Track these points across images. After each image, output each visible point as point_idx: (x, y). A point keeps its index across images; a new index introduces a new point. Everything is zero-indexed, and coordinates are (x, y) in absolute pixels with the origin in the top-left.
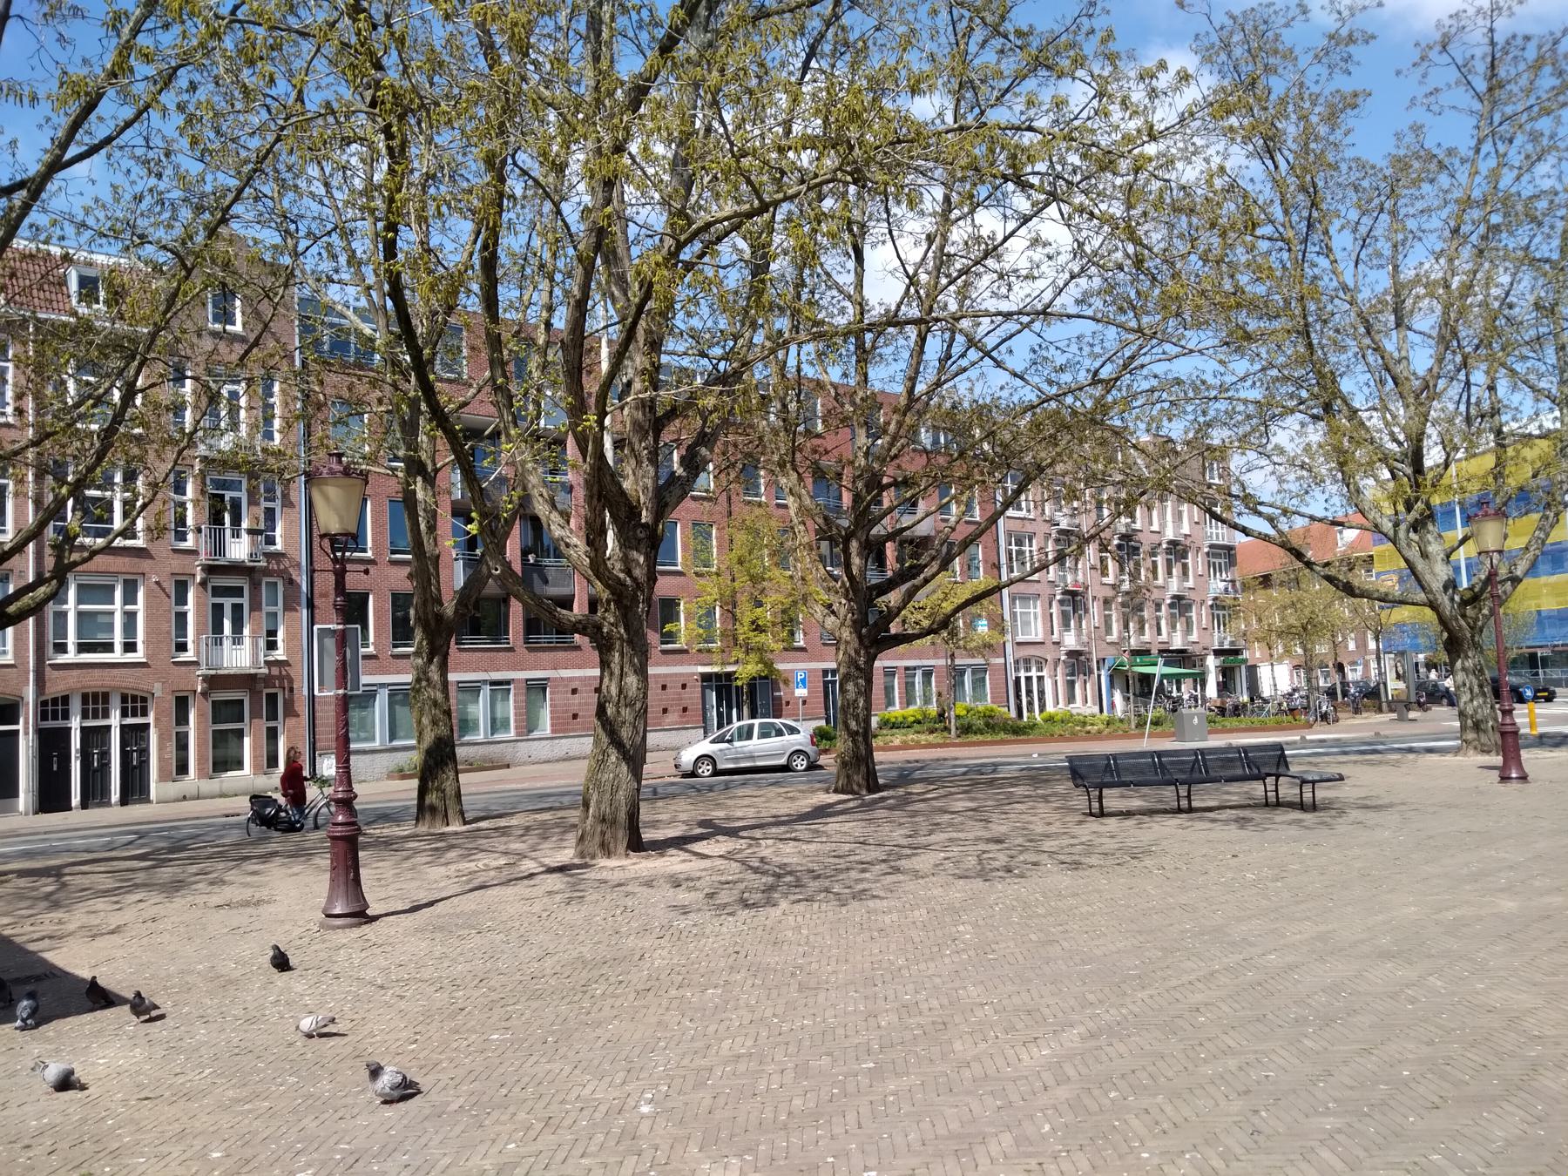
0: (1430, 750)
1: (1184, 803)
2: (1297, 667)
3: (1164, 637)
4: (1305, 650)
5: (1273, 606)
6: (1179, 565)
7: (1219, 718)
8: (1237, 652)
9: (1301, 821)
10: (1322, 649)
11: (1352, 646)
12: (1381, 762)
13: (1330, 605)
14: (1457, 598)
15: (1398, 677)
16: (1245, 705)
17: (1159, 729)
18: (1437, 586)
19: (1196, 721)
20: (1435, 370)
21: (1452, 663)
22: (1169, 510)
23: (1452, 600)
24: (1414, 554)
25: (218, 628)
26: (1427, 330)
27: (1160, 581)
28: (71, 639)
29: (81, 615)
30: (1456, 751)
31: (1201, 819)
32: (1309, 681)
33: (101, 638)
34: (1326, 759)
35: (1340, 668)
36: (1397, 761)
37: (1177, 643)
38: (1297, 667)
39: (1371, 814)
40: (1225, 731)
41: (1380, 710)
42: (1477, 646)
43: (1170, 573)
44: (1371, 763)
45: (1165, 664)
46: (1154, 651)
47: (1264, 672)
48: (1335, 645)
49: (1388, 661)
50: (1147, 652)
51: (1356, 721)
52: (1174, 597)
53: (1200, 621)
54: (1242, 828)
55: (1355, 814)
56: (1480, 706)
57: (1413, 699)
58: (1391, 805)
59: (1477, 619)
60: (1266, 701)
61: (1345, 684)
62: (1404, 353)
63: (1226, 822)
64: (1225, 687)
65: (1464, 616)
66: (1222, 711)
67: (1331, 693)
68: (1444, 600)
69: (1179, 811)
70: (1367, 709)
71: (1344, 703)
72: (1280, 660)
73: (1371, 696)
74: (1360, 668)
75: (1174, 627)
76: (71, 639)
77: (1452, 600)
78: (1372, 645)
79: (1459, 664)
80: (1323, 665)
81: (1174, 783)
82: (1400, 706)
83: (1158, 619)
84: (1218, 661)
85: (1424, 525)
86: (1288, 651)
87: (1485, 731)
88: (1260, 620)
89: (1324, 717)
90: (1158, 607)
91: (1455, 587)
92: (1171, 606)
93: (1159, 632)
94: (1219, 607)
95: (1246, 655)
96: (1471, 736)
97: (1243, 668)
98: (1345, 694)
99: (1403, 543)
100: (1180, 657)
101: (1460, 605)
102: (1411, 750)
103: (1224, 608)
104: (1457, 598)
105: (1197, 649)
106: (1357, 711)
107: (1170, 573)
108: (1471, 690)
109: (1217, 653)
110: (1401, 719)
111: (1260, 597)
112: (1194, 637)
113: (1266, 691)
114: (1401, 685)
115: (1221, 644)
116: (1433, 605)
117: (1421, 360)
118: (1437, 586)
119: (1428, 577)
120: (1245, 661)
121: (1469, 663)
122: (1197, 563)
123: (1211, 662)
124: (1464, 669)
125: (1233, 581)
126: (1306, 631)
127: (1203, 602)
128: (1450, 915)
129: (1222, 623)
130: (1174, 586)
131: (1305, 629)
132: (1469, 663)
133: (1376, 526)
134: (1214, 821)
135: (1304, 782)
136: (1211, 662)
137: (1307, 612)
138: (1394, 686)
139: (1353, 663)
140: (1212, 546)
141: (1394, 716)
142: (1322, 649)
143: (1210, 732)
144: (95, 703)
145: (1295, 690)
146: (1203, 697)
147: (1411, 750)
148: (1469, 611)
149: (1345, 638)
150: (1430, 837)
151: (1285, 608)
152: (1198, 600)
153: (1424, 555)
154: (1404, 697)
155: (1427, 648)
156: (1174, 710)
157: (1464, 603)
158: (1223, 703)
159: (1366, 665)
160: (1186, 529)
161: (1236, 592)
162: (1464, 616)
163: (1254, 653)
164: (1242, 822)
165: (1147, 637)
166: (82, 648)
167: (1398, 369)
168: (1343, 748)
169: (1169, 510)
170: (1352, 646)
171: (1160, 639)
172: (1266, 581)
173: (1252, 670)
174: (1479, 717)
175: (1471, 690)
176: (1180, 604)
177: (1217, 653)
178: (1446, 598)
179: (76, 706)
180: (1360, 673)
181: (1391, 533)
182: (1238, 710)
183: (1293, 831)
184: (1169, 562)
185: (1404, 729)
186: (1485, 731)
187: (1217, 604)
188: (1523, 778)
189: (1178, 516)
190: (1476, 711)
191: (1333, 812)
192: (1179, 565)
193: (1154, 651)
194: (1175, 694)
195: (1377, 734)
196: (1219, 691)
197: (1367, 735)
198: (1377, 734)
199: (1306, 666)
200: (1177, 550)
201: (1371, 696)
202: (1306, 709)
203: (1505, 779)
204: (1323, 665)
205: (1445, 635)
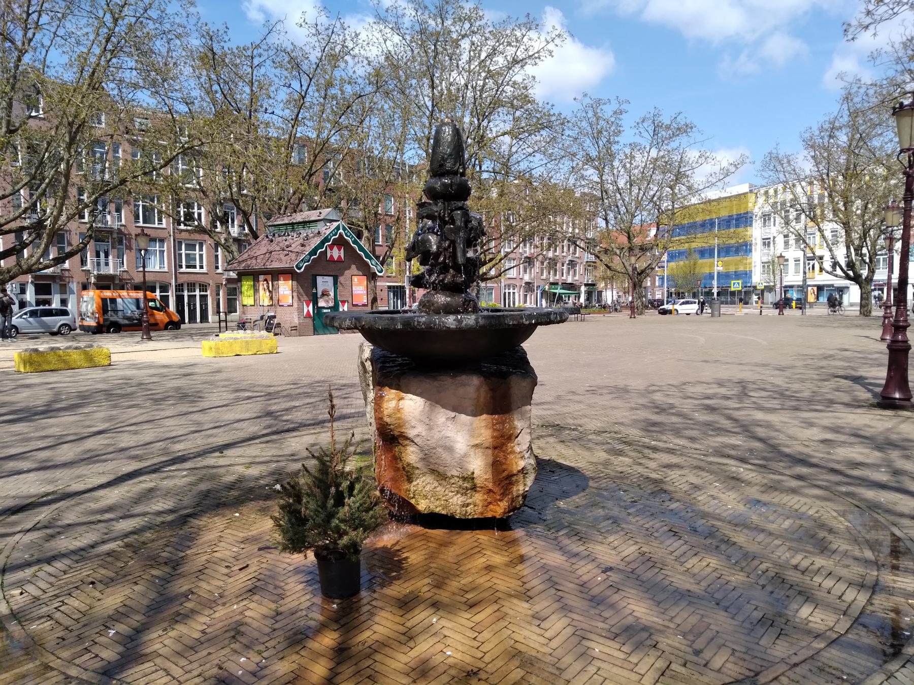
3: (564, 278)
28: (184, 264)
29: (186, 255)
33: (192, 263)
37: (570, 280)
50: (557, 284)
76: (184, 264)
100: (571, 287)
105: (577, 283)
109: (586, 285)
112: (576, 278)
123: (583, 289)
136: (583, 289)
144: (191, 286)
165: (557, 277)
166: (188, 267)
173: (600, 293)
177: (586, 285)
179: (185, 287)
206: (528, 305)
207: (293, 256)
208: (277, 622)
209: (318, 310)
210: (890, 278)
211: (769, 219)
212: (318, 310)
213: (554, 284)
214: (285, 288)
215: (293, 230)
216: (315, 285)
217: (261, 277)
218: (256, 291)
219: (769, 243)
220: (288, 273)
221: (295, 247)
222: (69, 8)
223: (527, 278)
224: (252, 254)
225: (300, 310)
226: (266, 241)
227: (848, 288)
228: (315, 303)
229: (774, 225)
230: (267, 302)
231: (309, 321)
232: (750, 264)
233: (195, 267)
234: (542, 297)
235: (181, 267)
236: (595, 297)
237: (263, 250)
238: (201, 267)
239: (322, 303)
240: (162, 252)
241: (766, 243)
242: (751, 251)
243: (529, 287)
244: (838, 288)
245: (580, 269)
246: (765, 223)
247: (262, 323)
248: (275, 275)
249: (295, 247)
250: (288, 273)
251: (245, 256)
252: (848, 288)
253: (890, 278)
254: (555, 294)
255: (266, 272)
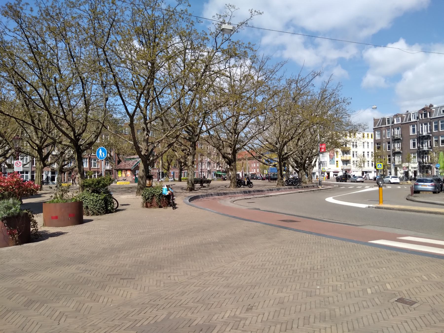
25: (106, 165)
28: (93, 165)
29: (94, 163)
33: (95, 165)
50: (220, 171)
76: (93, 165)
166: (94, 166)
206: (209, 178)
207: (131, 166)
209: (136, 178)
212: (136, 178)
214: (129, 173)
215: (130, 160)
216: (135, 172)
217: (123, 171)
218: (122, 173)
220: (130, 170)
221: (131, 164)
223: (208, 169)
224: (121, 165)
225: (132, 178)
226: (124, 162)
228: (135, 176)
230: (124, 176)
231: (134, 180)
233: (96, 166)
234: (214, 176)
235: (92, 166)
237: (123, 164)
238: (98, 166)
239: (137, 176)
240: (86, 162)
243: (209, 172)
247: (247, 25)
248: (127, 170)
249: (131, 164)
250: (130, 170)
251: (119, 166)
255: (124, 169)
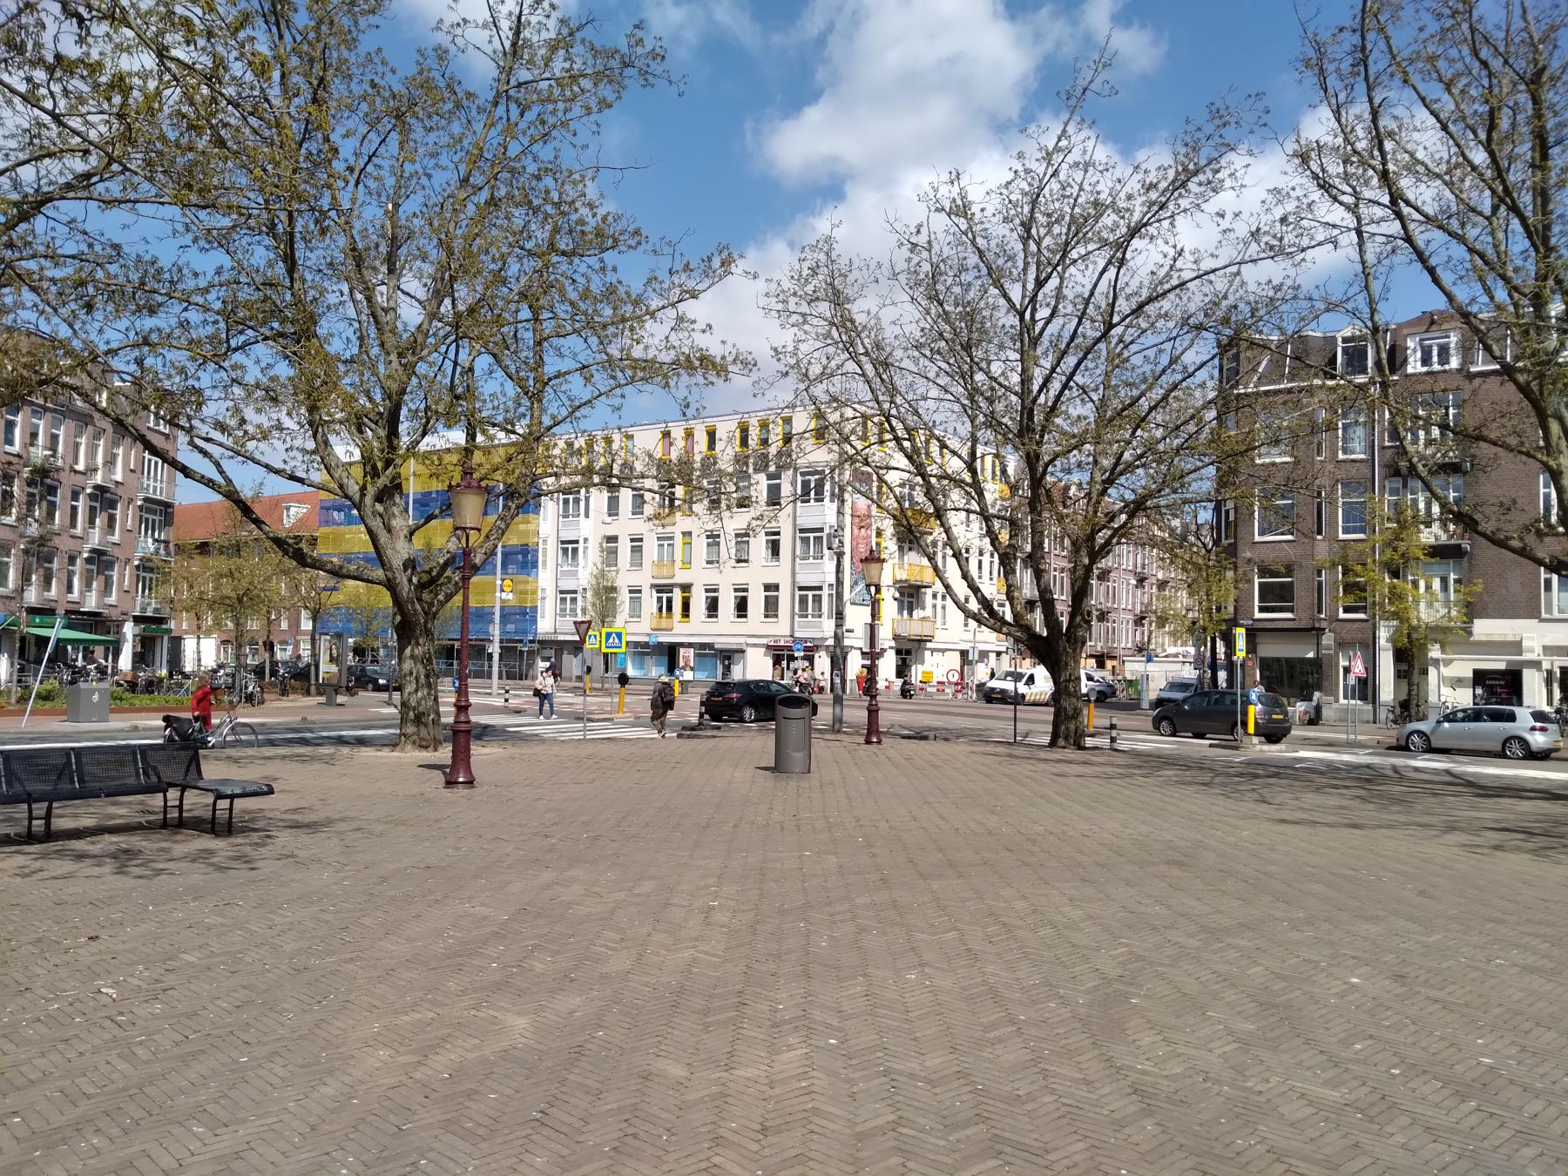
0: (361, 742)
1: (38, 825)
2: (225, 642)
3: (75, 595)
4: (237, 625)
5: (206, 574)
6: (105, 515)
7: (128, 695)
8: (161, 621)
9: (210, 852)
10: (254, 625)
11: (284, 625)
12: (313, 758)
13: (268, 579)
14: (415, 580)
15: (332, 660)
16: (161, 680)
17: (48, 705)
18: (397, 563)
19: (96, 697)
20: (425, 326)
21: (401, 651)
22: (100, 450)
23: (410, 581)
24: (376, 524)
26: (203, 663)
27: (79, 531)
30: (393, 744)
31: (60, 854)
32: (238, 657)
34: (250, 751)
35: (270, 646)
36: (332, 756)
37: (91, 603)
38: (225, 642)
39: (304, 838)
40: (134, 709)
41: (308, 693)
42: (428, 633)
43: (92, 522)
44: (300, 758)
45: (65, 627)
46: (61, 611)
47: (189, 645)
48: (270, 622)
49: (324, 642)
50: (51, 612)
51: (283, 704)
52: (93, 551)
53: (121, 581)
54: (120, 871)
55: (284, 839)
56: (423, 698)
57: (344, 683)
58: (328, 822)
59: (431, 605)
60: (186, 676)
61: (274, 664)
62: (392, 304)
63: (97, 858)
64: (141, 659)
65: (420, 600)
66: (132, 686)
67: (259, 671)
68: (402, 579)
69: (30, 838)
70: (294, 690)
71: (271, 684)
72: (208, 633)
73: (301, 678)
74: (290, 648)
75: (88, 585)
77: (410, 581)
78: (307, 625)
79: (408, 651)
80: (253, 642)
81: (30, 799)
82: (329, 690)
83: (70, 575)
84: (137, 630)
85: (391, 497)
86: (218, 624)
87: (426, 725)
88: (191, 587)
89: (249, 698)
90: (72, 560)
91: (414, 568)
92: (89, 561)
93: (70, 589)
94: (145, 569)
95: (172, 625)
96: (410, 729)
97: (166, 638)
98: (274, 673)
99: (368, 511)
100: (94, 621)
101: (417, 587)
102: (341, 741)
103: (151, 570)
104: (415, 580)
105: (115, 614)
106: (284, 693)
107: (91, 522)
108: (417, 679)
109: (137, 620)
110: (330, 703)
111: (196, 565)
112: (113, 599)
113: (189, 667)
114: (334, 668)
115: (144, 609)
116: (391, 585)
117: (411, 315)
118: (397, 563)
119: (389, 552)
120: (169, 631)
121: (419, 651)
122: (126, 516)
123: (129, 629)
124: (412, 657)
125: (166, 542)
126: (240, 604)
127: (128, 561)
128: (441, 1063)
129: (148, 586)
130: (95, 538)
131: (240, 600)
132: (419, 651)
133: (341, 487)
134: (80, 857)
135: (220, 796)
136: (129, 629)
137: (245, 584)
138: (326, 668)
139: (284, 642)
140: (146, 500)
141: (322, 699)
142: (254, 625)
143: (112, 711)
145: (221, 666)
146: (115, 667)
147: (341, 741)
148: (426, 596)
149: (278, 618)
150: (384, 879)
151: (222, 576)
152: (122, 557)
153: (389, 530)
154: (335, 681)
155: (358, 633)
156: (73, 682)
157: (422, 586)
158: (135, 677)
159: (297, 645)
160: (119, 477)
161: (168, 554)
162: (420, 600)
163: (179, 624)
164: (123, 858)
165: (53, 592)
167: (384, 318)
168: (268, 738)
169: (100, 450)
170: (284, 625)
171: (70, 597)
172: (203, 548)
173: (176, 642)
174: (421, 709)
175: (417, 679)
176: (101, 561)
177: (137, 620)
178: (405, 579)
180: (289, 653)
181: (357, 497)
182: (152, 686)
183: (197, 875)
184: (92, 510)
185: (331, 715)
186: (426, 725)
187: (146, 566)
188: (470, 783)
189: (110, 462)
190: (419, 703)
191: (255, 837)
192: (105, 515)
193: (61, 611)
194: (80, 663)
195: (304, 719)
196: (134, 662)
197: (293, 719)
198: (304, 719)
199: (236, 641)
200: (104, 499)
201: (301, 678)
202: (231, 688)
203: (450, 783)
204: (253, 642)
205: (398, 618)
208: (708, 1159)
210: (462, 692)
211: (577, 501)
213: (43, 612)
219: (575, 550)
222: (1533, 355)
227: (743, 651)
229: (587, 515)
232: (534, 592)
236: (163, 651)
241: (569, 548)
242: (535, 565)
244: (722, 651)
245: (123, 576)
246: (566, 509)
252: (743, 651)
253: (462, 692)
254: (42, 642)
